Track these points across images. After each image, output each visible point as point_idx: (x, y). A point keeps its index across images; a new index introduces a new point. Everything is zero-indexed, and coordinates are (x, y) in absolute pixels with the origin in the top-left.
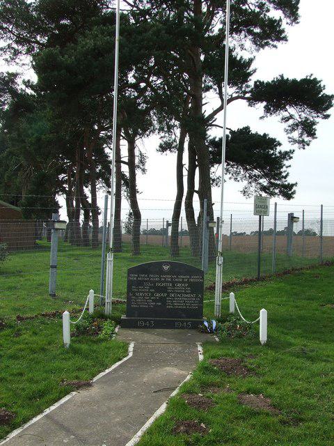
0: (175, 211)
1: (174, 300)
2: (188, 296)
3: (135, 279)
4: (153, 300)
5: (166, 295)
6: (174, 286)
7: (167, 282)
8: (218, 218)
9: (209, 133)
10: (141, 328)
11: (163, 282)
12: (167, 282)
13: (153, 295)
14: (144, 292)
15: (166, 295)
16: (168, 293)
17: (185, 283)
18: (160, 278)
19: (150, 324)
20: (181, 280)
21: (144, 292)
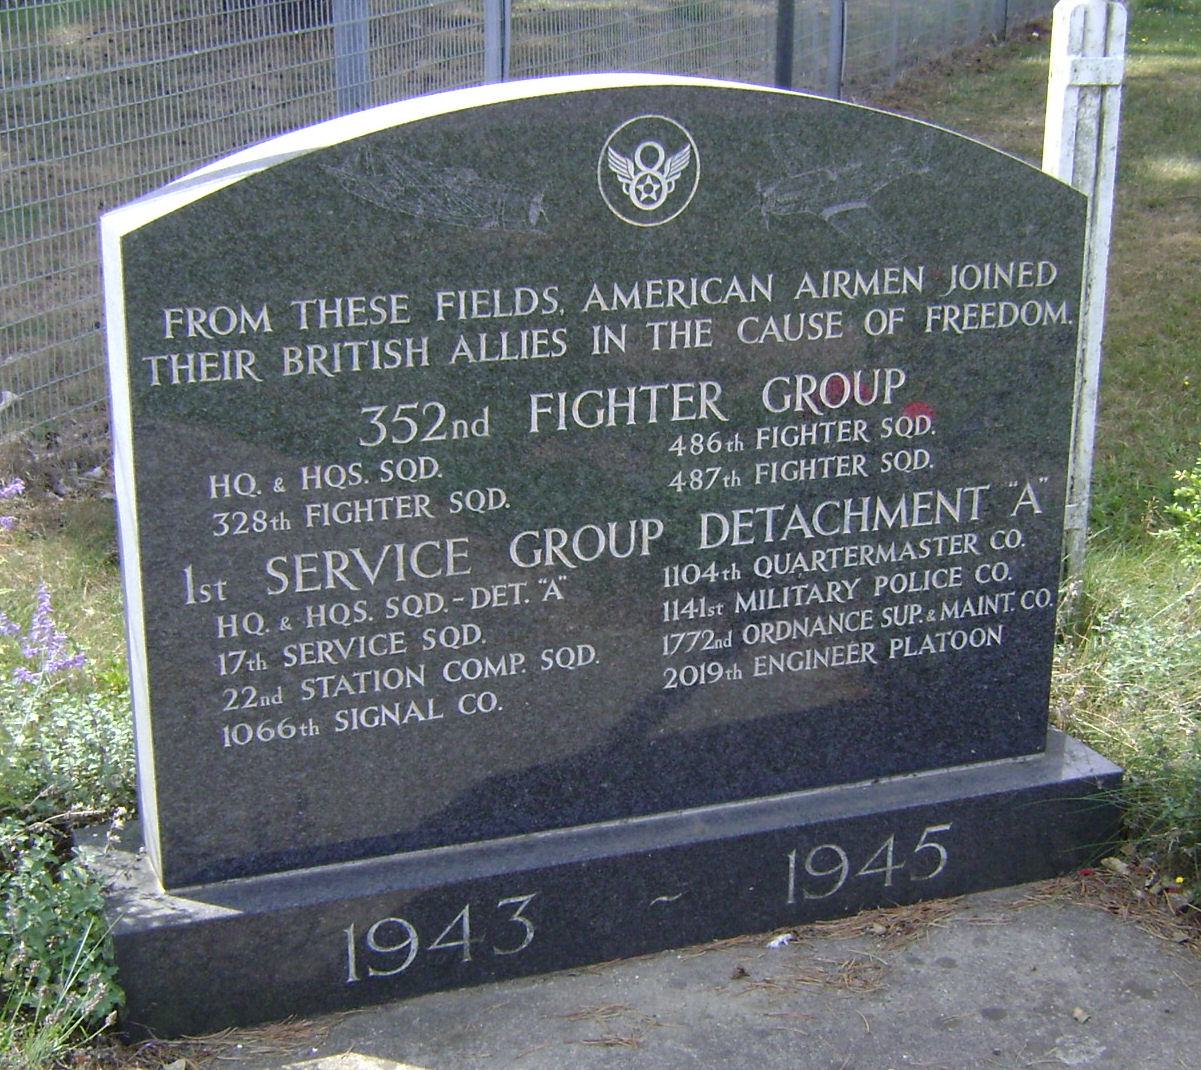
0: (1103, 34)
1: (750, 584)
2: (907, 513)
3: (241, 366)
4: (486, 618)
5: (649, 530)
6: (743, 417)
7: (668, 367)
8: (692, 1042)
9: (1064, 772)
10: (374, 992)
11: (615, 373)
12: (668, 367)
13: (488, 558)
14: (370, 538)
15: (649, 530)
16: (683, 513)
17: (873, 354)
18: (578, 325)
19: (494, 926)
20: (826, 328)
21: (370, 538)
